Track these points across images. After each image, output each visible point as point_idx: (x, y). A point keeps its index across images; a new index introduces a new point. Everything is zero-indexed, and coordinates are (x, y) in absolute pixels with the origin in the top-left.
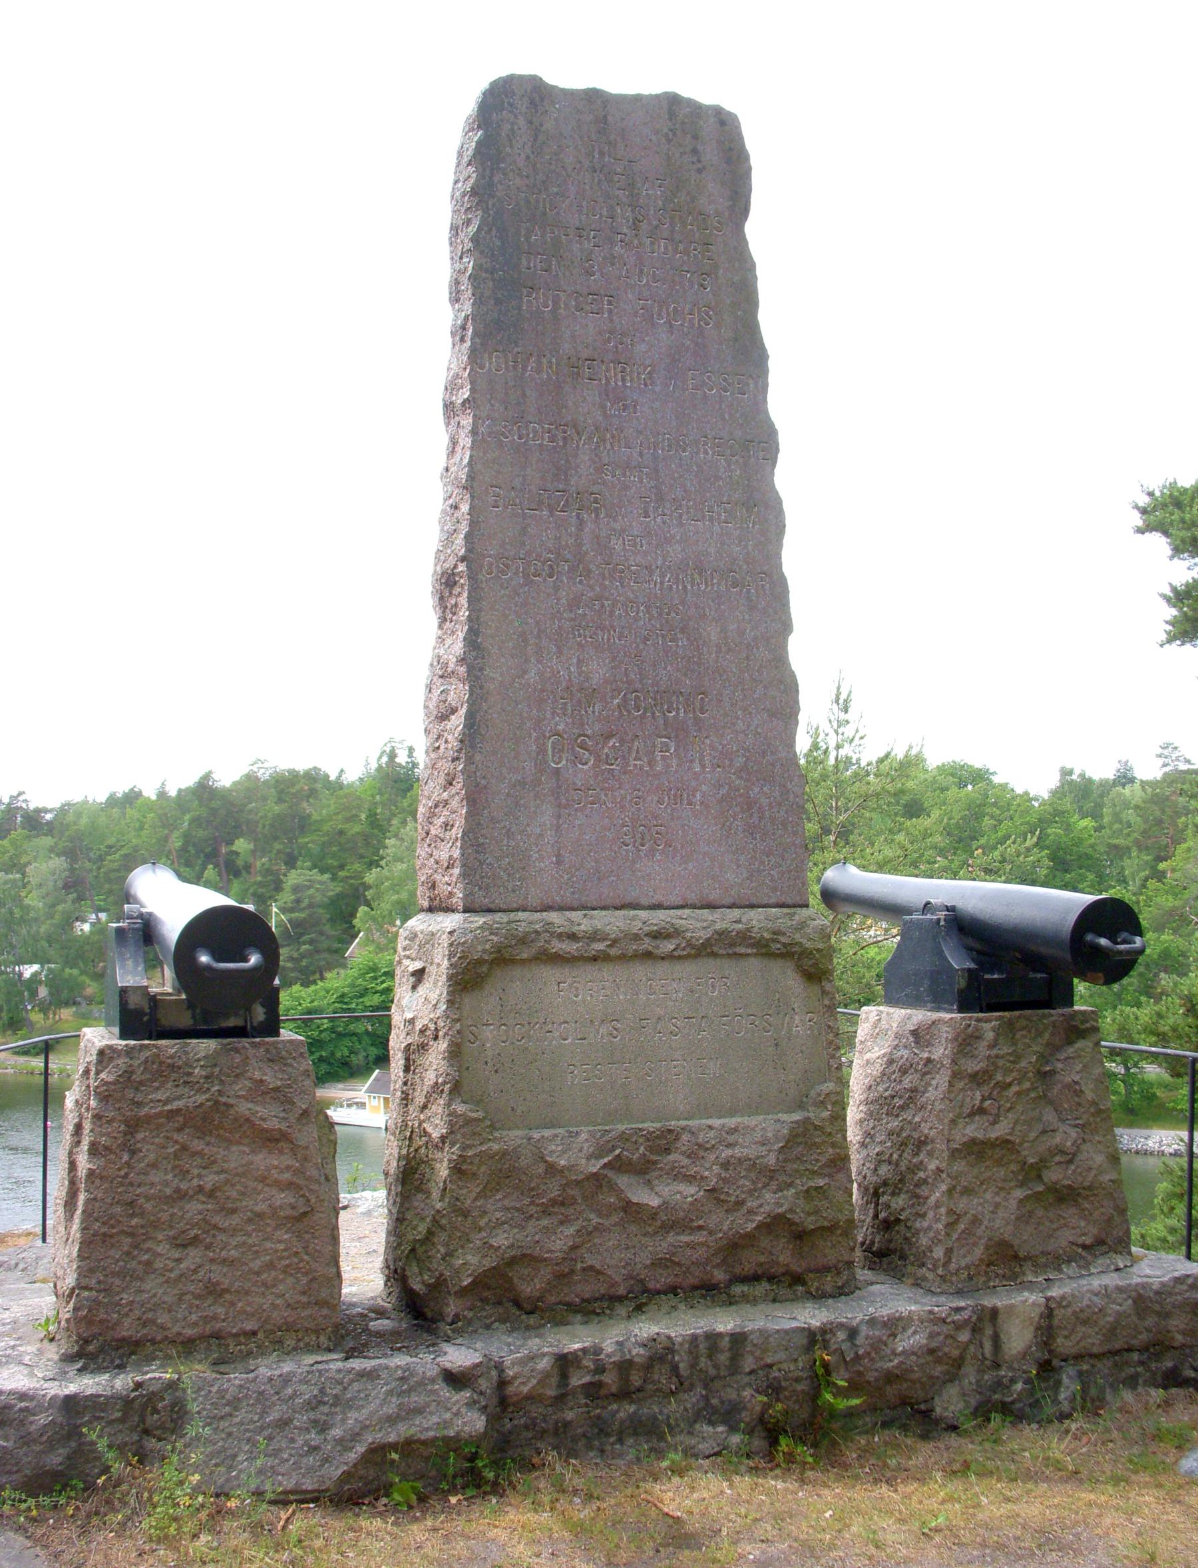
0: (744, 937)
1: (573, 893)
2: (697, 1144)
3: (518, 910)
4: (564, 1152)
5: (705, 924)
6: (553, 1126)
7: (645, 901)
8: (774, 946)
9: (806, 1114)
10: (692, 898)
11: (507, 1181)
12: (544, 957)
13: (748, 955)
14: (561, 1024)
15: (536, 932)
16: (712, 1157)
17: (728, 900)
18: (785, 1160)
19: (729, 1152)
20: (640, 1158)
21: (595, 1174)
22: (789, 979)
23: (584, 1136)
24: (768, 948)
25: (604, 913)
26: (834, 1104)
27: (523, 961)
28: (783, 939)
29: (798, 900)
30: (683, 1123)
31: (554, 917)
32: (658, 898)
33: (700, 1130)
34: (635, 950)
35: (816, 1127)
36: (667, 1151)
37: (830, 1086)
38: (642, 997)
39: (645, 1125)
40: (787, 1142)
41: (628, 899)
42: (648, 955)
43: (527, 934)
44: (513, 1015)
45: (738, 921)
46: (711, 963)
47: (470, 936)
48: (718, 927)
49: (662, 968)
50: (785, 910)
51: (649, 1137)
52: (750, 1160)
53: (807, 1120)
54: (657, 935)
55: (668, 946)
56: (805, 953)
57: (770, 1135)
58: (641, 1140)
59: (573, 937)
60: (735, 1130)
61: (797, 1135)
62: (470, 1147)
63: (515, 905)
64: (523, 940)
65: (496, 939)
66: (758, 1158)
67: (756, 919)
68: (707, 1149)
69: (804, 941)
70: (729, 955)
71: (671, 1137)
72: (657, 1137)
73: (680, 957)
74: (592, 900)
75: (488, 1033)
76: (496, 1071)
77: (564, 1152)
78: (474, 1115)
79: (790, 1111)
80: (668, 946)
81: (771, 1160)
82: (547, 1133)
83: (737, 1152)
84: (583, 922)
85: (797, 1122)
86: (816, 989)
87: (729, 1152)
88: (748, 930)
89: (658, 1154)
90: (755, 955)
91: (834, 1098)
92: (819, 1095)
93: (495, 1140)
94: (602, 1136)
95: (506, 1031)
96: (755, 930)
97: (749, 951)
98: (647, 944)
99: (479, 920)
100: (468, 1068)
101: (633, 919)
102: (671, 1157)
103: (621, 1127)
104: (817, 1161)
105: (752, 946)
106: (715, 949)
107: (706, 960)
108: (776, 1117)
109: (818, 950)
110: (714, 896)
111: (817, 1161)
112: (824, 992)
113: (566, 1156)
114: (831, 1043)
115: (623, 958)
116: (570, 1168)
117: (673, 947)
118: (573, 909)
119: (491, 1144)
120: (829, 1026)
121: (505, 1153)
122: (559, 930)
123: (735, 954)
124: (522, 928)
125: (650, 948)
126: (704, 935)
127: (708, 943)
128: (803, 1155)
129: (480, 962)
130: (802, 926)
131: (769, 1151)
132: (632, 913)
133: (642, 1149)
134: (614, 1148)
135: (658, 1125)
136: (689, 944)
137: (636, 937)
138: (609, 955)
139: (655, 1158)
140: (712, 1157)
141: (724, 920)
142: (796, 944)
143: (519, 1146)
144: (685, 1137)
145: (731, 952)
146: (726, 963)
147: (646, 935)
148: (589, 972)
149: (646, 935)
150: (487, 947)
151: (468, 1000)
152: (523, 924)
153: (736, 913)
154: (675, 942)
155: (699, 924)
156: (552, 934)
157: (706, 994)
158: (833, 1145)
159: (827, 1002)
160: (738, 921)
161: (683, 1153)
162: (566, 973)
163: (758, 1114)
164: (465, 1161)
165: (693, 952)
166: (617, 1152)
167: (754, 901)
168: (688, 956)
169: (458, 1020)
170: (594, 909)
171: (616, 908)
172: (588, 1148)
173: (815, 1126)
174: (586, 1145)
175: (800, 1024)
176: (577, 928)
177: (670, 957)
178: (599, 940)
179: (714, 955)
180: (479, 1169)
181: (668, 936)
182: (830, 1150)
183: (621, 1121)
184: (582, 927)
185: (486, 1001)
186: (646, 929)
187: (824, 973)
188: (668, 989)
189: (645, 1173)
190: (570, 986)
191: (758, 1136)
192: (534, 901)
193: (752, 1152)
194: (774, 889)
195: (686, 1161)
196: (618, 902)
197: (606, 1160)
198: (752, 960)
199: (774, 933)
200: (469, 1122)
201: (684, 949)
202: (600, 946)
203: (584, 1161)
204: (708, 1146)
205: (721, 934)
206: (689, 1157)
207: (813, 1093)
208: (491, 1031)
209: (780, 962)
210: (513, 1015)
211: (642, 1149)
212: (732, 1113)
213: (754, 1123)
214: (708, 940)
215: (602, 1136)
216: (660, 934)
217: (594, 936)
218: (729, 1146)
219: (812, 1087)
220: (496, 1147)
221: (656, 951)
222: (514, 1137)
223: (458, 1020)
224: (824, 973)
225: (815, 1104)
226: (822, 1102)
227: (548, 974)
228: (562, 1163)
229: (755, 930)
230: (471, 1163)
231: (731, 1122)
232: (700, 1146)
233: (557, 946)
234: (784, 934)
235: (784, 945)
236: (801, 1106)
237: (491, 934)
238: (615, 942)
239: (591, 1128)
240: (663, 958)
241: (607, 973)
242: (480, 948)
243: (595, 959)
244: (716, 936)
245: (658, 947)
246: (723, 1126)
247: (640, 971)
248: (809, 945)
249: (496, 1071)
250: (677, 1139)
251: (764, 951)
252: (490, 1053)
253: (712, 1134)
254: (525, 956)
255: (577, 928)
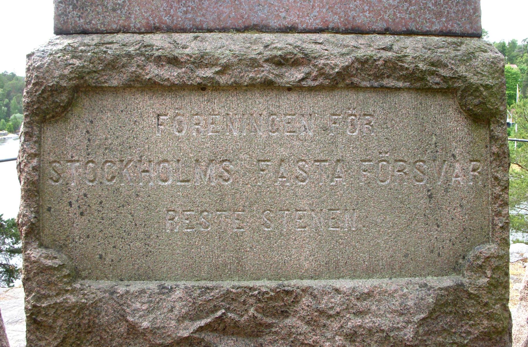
0: (393, 66)
1: (186, 12)
2: (318, 310)
3: (118, 32)
4: (149, 311)
5: (344, 50)
6: (139, 278)
7: (274, 23)
8: (432, 80)
9: (460, 279)
10: (335, 20)
11: (89, 337)
12: (138, 85)
13: (399, 89)
14: (159, 163)
15: (129, 55)
16: (336, 325)
17: (381, 25)
18: (428, 333)
19: (358, 321)
20: (249, 321)
21: (187, 338)
22: (448, 120)
23: (178, 293)
24: (421, 82)
25: (220, 35)
26: (494, 270)
27: (115, 90)
28: (442, 72)
29: (467, 27)
30: (306, 283)
31: (157, 40)
32: (292, 19)
33: (324, 293)
34: (252, 79)
35: (470, 296)
36: (285, 314)
37: (490, 248)
38: (262, 134)
39: (258, 284)
40: (431, 313)
41: (255, 20)
42: (268, 85)
43: (117, 57)
44: (101, 151)
45: (389, 49)
46: (352, 97)
47: (47, 60)
48: (360, 54)
49: (288, 101)
50: (450, 39)
51: (261, 297)
52: (383, 331)
53: (460, 286)
54: (282, 61)
55: (295, 75)
56: (470, 90)
57: (410, 303)
58: (251, 301)
59: (174, 61)
60: (369, 295)
61: (446, 304)
62: (46, 297)
63: (114, 26)
64: (113, 65)
65: (77, 62)
66: (392, 329)
67: (411, 47)
68: (331, 316)
69: (469, 75)
70: (372, 88)
71: (289, 299)
72: (271, 298)
73: (311, 89)
74: (210, 21)
75: (73, 170)
76: (82, 214)
77: (149, 311)
78: (49, 263)
79: (442, 273)
80: (295, 75)
81: (409, 333)
82: (135, 287)
83: (368, 321)
84: (190, 45)
85: (446, 289)
86: (484, 133)
87: (358, 321)
88: (400, 59)
89: (273, 315)
90: (409, 89)
91: (495, 263)
92: (478, 258)
93: (73, 291)
94: (202, 294)
95: (94, 170)
96: (409, 59)
97: (400, 84)
98: (268, 72)
99: (65, 41)
100: (49, 209)
101: (255, 42)
102: (288, 321)
103: (227, 284)
104: (469, 333)
105: (405, 78)
106: (355, 80)
107: (345, 93)
108: (423, 280)
109: (487, 87)
110: (363, 19)
111: (469, 333)
112: (493, 138)
113: (151, 317)
114: (497, 197)
115: (236, 87)
116: (153, 331)
117: (300, 76)
118: (184, 30)
119: (68, 296)
120: (496, 178)
121: (82, 308)
122: (157, 54)
123: (382, 87)
124: (113, 50)
125: (271, 77)
126: (342, 62)
127: (345, 73)
128: (451, 326)
129: (56, 90)
130: (470, 56)
131: (408, 322)
132: (256, 35)
133: (252, 311)
134: (216, 309)
135: (273, 284)
136: (322, 73)
137: (254, 63)
138: (218, 83)
139: (269, 320)
140: (336, 325)
141: (367, 47)
142: (460, 77)
143: (100, 300)
144: (306, 300)
145: (376, 84)
146: (372, 98)
147: (266, 61)
148: (197, 102)
149: (266, 61)
150: (66, 72)
151: (50, 134)
152: (115, 46)
153: (388, 39)
154: (305, 69)
155: (335, 51)
156: (148, 58)
157: (344, 133)
158: (489, 317)
159: (495, 149)
160: (389, 49)
161: (302, 318)
162: (166, 104)
163: (401, 275)
164: (39, 312)
165: (327, 82)
166: (219, 313)
167: (412, 26)
168: (320, 88)
169: (35, 155)
170: (210, 31)
171: (238, 30)
172: (180, 308)
173: (470, 294)
174: (178, 305)
175: (461, 174)
176: (180, 51)
177: (297, 88)
178: (206, 66)
179: (354, 87)
180: (55, 321)
181: (296, 63)
182: (485, 322)
183: (230, 277)
184: (187, 51)
185: (70, 136)
186: (268, 53)
187: (494, 115)
188: (298, 125)
189: (258, 336)
190: (173, 119)
191: (395, 304)
192: (136, 22)
193: (385, 323)
194: (440, 15)
195: (304, 328)
196: (240, 23)
197: (203, 323)
198: (405, 96)
199: (433, 64)
200: (44, 270)
201: (315, 79)
202: (208, 73)
203: (173, 323)
204: (331, 312)
205: (364, 62)
206: (308, 323)
207: (471, 255)
208: (77, 169)
209: (440, 99)
210: (101, 151)
211: (252, 311)
212: (370, 272)
213: (393, 287)
214: (346, 68)
215: (202, 294)
216: (287, 60)
217: (201, 61)
218: (359, 313)
219: (471, 247)
220: (72, 299)
221: (278, 80)
222: (95, 288)
223: (35, 155)
224: (494, 115)
225: (471, 268)
226: (481, 266)
227: (146, 105)
228: (145, 324)
229: (409, 59)
230: (46, 315)
231: (365, 284)
232: (322, 312)
233: (153, 71)
234: (446, 66)
235: (445, 79)
236: (456, 269)
237: (73, 57)
238: (225, 68)
239: (190, 284)
240: (289, 89)
241: (219, 105)
242: (57, 73)
243: (202, 88)
244: (356, 65)
245: (281, 76)
246: (354, 290)
247: (260, 103)
248: (474, 80)
249: (82, 214)
250: (296, 301)
251: (418, 85)
252: (74, 194)
253: (338, 299)
254: (115, 83)
255: (180, 51)
